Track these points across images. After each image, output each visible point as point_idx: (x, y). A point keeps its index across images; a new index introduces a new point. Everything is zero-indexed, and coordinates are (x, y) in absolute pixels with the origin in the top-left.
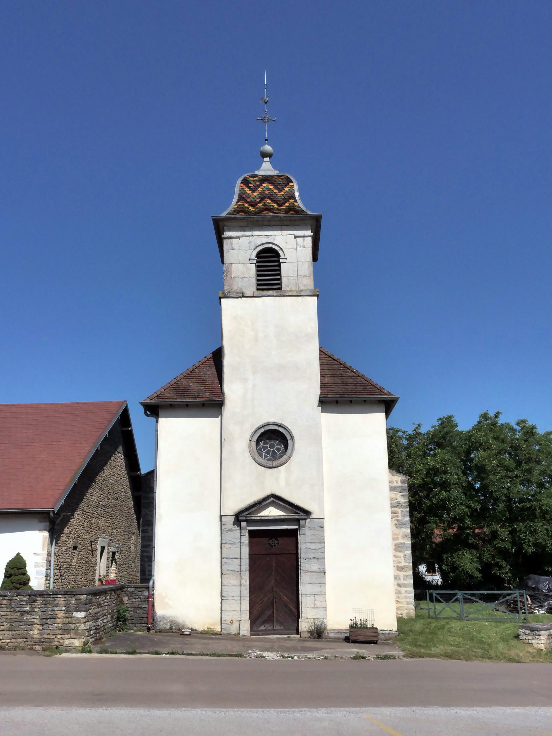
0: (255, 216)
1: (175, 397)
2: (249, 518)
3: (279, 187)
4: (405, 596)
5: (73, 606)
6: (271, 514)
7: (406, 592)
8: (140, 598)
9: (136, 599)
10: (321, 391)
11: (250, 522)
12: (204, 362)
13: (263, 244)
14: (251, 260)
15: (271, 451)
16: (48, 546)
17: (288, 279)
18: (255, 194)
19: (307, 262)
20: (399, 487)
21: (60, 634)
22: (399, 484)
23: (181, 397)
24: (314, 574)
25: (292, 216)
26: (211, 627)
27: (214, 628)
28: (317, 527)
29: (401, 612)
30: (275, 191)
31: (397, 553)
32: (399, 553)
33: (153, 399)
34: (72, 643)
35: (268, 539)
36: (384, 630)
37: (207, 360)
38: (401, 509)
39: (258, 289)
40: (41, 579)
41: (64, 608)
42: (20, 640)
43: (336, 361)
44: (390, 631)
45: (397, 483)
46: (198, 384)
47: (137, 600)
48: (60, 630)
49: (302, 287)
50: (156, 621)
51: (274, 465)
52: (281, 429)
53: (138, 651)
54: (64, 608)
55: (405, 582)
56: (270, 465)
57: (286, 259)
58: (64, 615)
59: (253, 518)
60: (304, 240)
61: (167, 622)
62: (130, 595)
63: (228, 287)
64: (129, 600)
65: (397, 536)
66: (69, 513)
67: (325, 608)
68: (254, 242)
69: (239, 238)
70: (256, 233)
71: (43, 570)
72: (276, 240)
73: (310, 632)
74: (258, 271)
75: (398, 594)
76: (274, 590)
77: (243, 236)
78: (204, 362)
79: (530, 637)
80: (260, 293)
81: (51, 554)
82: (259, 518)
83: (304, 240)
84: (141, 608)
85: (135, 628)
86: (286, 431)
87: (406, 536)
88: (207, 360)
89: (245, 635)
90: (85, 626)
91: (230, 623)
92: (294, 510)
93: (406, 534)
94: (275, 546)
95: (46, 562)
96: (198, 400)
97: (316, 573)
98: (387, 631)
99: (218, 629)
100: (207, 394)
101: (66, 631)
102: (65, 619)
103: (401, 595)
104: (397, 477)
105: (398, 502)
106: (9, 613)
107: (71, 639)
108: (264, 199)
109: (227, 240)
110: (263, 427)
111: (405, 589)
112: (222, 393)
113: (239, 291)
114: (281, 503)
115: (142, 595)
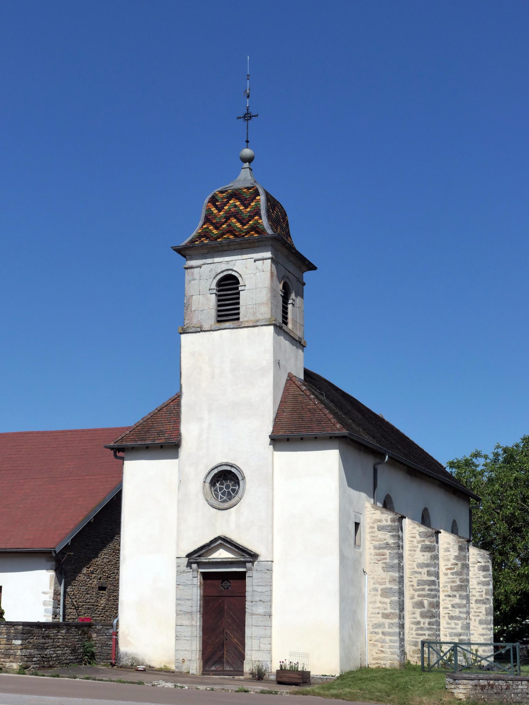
0: (211, 243)
1: (137, 439)
2: (198, 561)
3: (245, 202)
4: (390, 646)
6: (220, 557)
7: (391, 641)
8: (107, 635)
9: (103, 636)
10: (273, 428)
11: (200, 564)
12: (174, 400)
13: (222, 272)
14: (210, 290)
15: (227, 493)
16: (54, 585)
17: (246, 308)
18: (222, 213)
19: (265, 287)
20: (389, 526)
21: (3, 658)
22: (389, 523)
23: (142, 439)
24: (259, 616)
25: (248, 240)
26: (167, 666)
27: (169, 666)
28: (264, 570)
29: (385, 662)
30: (242, 208)
31: (382, 599)
32: (385, 599)
33: (117, 442)
34: (12, 666)
35: (221, 581)
36: (326, 676)
37: (177, 398)
38: (390, 551)
39: (219, 321)
40: (48, 617)
41: (5, 636)
43: (303, 392)
44: (332, 676)
45: (387, 521)
46: (161, 424)
47: (104, 637)
48: (3, 654)
49: (260, 317)
50: (119, 657)
51: (225, 507)
52: (233, 470)
53: (61, 675)
54: (5, 636)
55: (390, 630)
56: (221, 507)
57: (245, 286)
58: (5, 642)
59: (202, 560)
60: (263, 263)
61: (129, 659)
62: (98, 632)
63: (188, 322)
64: (97, 637)
65: (384, 581)
66: (71, 552)
67: (270, 651)
68: (215, 270)
69: (200, 267)
70: (217, 260)
71: (50, 608)
72: (236, 265)
73: (252, 673)
74: (219, 301)
75: (382, 643)
76: (225, 632)
77: (204, 264)
78: (174, 400)
79: (453, 686)
81: (60, 593)
82: (207, 560)
83: (263, 263)
84: (107, 644)
85: (103, 663)
86: (238, 471)
87: (394, 580)
88: (177, 398)
89: (194, 674)
90: (21, 652)
91: (182, 662)
92: (241, 552)
93: (394, 578)
94: (227, 588)
95: (53, 601)
96: (156, 442)
97: (261, 616)
98: (329, 676)
99: (173, 667)
100: (166, 435)
102: (6, 645)
103: (385, 644)
104: (387, 515)
105: (387, 542)
107: (11, 663)
108: (229, 219)
109: (189, 270)
110: (216, 467)
111: (390, 638)
112: (179, 435)
113: (198, 325)
114: (228, 545)
115: (108, 633)
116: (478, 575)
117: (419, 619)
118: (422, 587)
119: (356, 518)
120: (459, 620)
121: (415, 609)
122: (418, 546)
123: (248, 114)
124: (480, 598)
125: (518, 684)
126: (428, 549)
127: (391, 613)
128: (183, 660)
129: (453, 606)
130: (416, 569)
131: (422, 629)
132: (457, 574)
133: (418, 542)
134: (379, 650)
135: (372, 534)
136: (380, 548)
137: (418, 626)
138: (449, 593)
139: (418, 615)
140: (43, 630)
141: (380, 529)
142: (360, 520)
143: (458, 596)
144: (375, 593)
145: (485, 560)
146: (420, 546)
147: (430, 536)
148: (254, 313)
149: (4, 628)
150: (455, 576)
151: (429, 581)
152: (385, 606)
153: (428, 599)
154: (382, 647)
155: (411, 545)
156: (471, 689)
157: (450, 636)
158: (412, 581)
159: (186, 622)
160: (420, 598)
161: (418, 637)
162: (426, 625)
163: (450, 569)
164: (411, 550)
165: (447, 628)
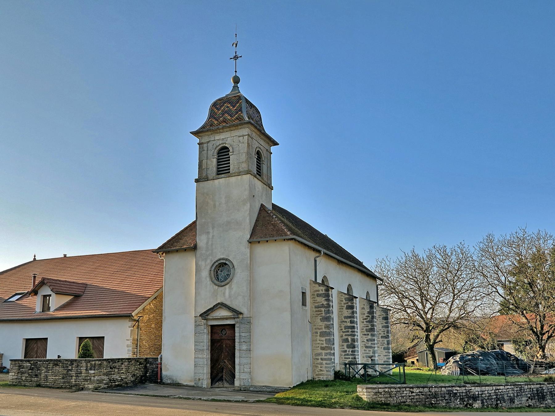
4: (326, 366)
5: (89, 368)
20: (323, 294)
40: (130, 354)
42: (67, 384)
45: (322, 291)
49: (241, 170)
55: (325, 357)
59: (209, 318)
65: (321, 327)
80: (218, 176)
101: (86, 380)
106: (63, 370)
111: (326, 362)
116: (382, 322)
117: (346, 349)
118: (347, 330)
119: (303, 290)
120: (371, 348)
121: (344, 343)
122: (344, 306)
123: (236, 56)
124: (384, 335)
125: (404, 390)
126: (350, 308)
127: (326, 346)
128: (199, 379)
129: (367, 340)
130: (344, 320)
131: (348, 355)
132: (369, 322)
133: (344, 304)
134: (319, 369)
135: (314, 299)
136: (319, 307)
137: (345, 353)
138: (365, 333)
139: (345, 347)
140: (111, 363)
141: (319, 295)
142: (306, 291)
143: (370, 334)
144: (316, 335)
145: (386, 314)
146: (346, 306)
147: (351, 300)
148: (239, 168)
149: (84, 363)
150: (368, 323)
151: (351, 326)
152: (322, 342)
153: (351, 337)
154: (321, 367)
155: (340, 306)
156: (373, 395)
157: (366, 357)
158: (341, 327)
159: (200, 356)
160: (346, 337)
161: (345, 359)
162: (350, 353)
163: (365, 319)
164: (341, 309)
165: (364, 353)
